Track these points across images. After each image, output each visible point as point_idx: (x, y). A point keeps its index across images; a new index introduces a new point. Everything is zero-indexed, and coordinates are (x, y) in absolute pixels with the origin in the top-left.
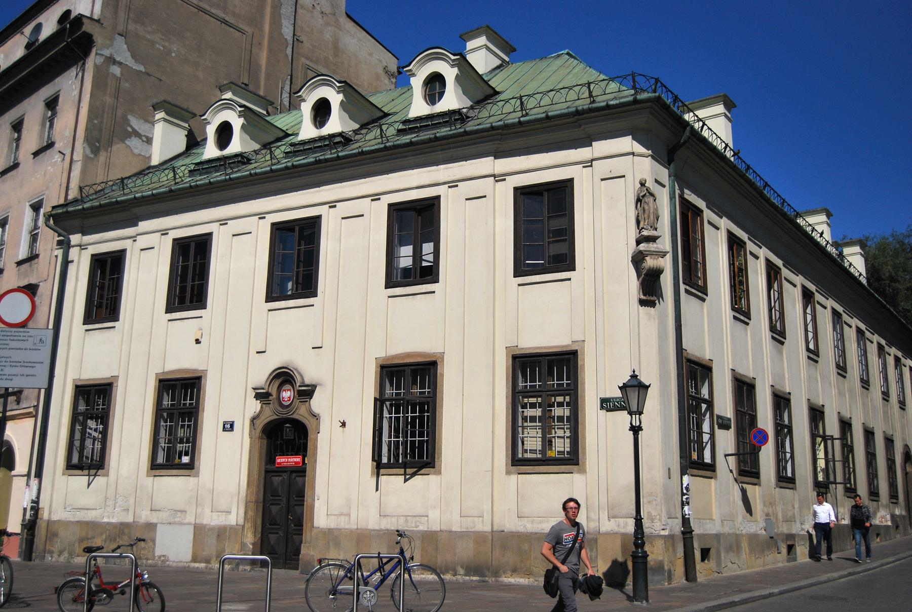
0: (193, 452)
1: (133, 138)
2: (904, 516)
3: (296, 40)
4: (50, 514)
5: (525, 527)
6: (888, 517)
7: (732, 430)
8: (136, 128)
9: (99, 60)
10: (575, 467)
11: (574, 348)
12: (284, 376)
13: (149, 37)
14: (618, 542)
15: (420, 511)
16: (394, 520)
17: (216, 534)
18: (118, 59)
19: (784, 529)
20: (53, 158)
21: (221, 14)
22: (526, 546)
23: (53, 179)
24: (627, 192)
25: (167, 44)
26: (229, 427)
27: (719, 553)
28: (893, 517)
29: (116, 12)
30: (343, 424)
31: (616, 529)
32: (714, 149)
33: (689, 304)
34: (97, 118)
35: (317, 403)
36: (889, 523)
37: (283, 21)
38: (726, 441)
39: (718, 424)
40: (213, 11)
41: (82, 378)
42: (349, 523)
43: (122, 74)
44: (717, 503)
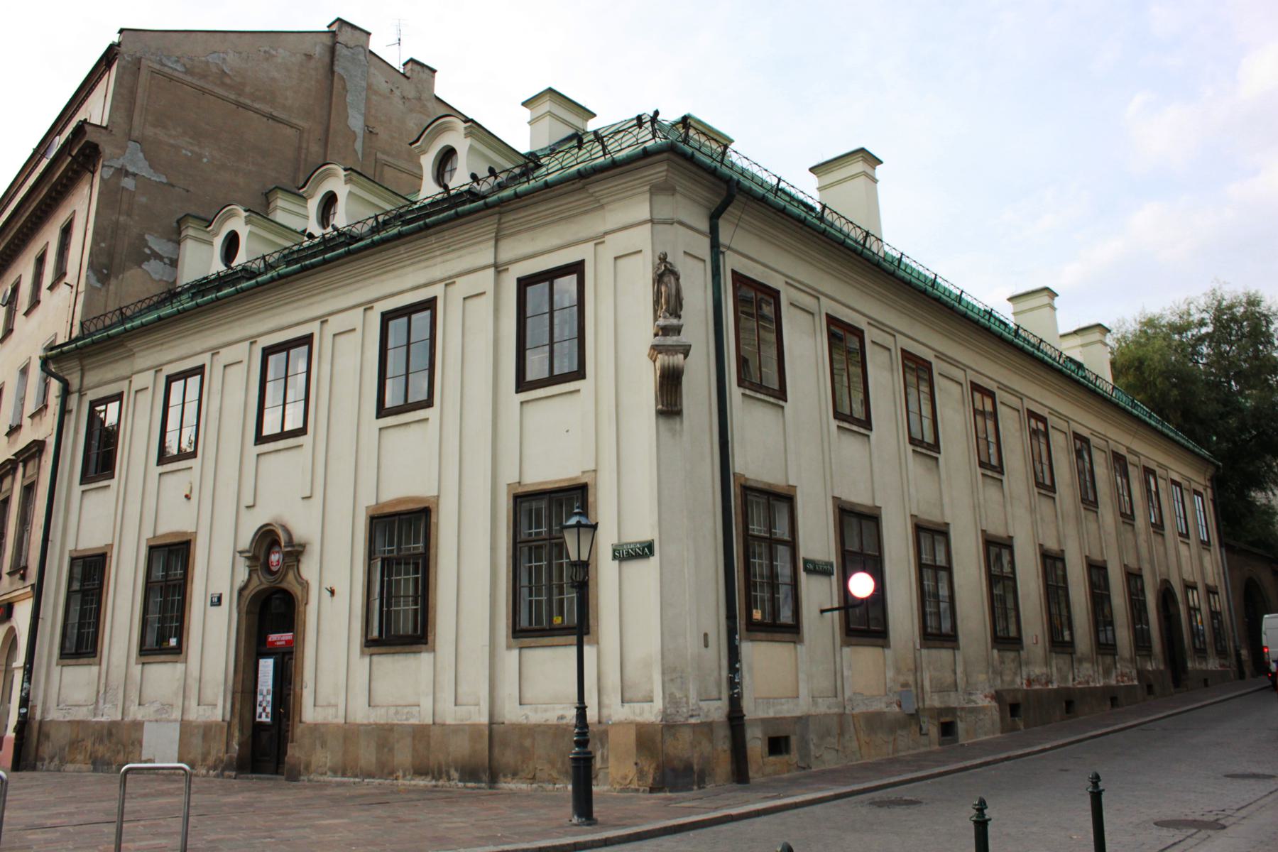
0: (180, 633)
1: (152, 261)
2: (1161, 672)
3: (370, 132)
4: (43, 712)
5: (527, 717)
6: (1134, 673)
7: (834, 578)
8: (156, 248)
9: (108, 173)
11: (583, 480)
12: (268, 538)
13: (172, 141)
14: (633, 737)
16: (383, 711)
17: (201, 731)
18: (131, 169)
19: (934, 701)
20: (63, 290)
21: (266, 108)
22: (528, 743)
23: (56, 316)
24: (641, 274)
25: (196, 149)
26: (217, 601)
27: (804, 743)
28: (1141, 674)
29: (130, 117)
30: (332, 592)
31: (632, 717)
33: (749, 417)
34: (104, 241)
35: (309, 569)
36: (1136, 683)
39: (806, 570)
40: (256, 105)
41: (81, 547)
42: (336, 717)
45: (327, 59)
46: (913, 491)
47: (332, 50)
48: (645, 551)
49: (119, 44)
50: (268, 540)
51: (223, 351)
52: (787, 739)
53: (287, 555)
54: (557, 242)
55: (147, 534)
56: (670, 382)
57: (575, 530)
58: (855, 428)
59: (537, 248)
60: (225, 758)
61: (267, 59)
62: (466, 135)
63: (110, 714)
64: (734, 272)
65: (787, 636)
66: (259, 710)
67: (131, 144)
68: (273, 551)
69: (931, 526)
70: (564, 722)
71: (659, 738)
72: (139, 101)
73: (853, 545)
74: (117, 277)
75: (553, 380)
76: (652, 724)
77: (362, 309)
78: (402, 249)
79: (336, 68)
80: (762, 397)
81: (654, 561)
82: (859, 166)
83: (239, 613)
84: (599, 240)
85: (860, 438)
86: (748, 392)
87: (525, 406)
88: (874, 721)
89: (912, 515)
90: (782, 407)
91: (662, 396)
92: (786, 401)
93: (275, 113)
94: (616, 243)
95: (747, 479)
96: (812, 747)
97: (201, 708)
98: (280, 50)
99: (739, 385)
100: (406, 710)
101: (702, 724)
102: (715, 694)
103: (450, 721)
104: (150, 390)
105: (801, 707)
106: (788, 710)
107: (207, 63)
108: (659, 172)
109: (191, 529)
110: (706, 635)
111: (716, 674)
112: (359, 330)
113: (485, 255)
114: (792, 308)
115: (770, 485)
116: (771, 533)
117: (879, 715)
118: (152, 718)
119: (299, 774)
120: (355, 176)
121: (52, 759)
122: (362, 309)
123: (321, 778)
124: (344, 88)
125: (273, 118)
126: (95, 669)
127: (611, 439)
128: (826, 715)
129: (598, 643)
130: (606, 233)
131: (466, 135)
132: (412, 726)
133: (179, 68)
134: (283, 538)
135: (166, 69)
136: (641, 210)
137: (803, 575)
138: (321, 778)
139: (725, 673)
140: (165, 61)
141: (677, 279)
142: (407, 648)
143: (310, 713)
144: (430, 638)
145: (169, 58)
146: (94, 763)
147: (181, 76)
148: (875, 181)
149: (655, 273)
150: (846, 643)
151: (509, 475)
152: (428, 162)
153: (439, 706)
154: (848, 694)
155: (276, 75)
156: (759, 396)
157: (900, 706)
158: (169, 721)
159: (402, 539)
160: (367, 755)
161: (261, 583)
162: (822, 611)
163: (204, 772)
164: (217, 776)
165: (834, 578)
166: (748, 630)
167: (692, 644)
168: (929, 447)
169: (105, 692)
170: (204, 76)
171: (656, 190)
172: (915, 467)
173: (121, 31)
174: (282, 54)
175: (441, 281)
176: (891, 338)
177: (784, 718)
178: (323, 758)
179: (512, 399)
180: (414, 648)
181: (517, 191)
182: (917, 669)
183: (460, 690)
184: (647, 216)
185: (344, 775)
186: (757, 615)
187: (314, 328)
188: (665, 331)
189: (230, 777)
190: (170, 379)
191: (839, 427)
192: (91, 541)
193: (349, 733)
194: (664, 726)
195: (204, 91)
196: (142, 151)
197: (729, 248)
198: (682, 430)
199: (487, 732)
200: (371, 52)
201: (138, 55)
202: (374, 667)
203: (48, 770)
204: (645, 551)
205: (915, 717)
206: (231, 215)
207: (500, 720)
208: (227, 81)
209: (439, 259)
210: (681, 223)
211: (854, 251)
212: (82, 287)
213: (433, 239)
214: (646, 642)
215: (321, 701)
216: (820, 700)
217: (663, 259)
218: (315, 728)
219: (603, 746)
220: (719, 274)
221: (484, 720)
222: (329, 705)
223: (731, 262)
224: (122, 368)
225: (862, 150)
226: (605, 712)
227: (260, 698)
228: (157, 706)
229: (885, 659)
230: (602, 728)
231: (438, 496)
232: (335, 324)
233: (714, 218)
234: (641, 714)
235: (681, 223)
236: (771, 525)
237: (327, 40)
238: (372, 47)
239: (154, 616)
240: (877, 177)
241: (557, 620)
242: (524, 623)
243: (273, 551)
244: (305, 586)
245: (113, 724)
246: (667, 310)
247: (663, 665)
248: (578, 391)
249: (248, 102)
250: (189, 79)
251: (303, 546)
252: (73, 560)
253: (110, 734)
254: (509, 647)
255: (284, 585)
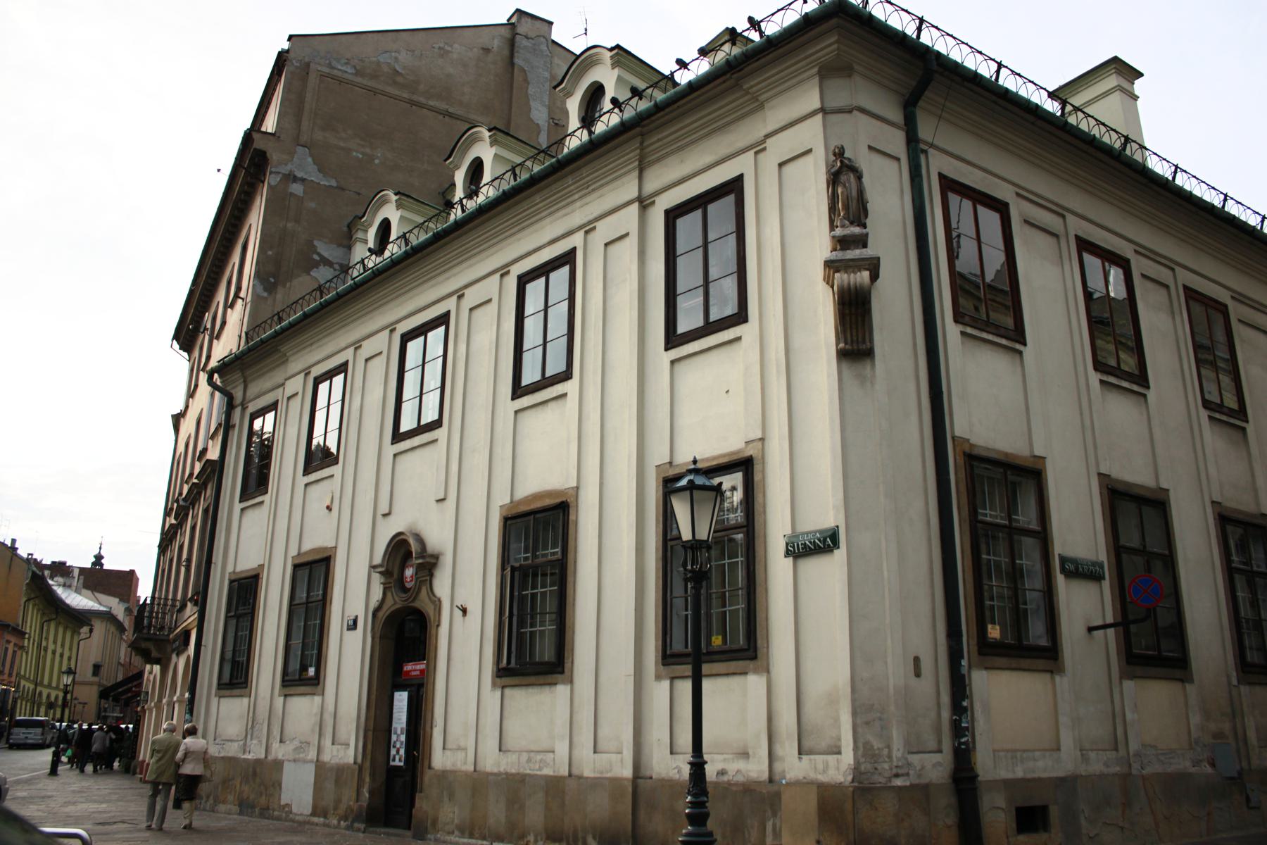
7: (1106, 584)
8: (326, 254)
10: (751, 664)
13: (342, 144)
15: (545, 745)
18: (299, 174)
21: (443, 106)
24: (811, 182)
25: (368, 150)
26: (353, 626)
29: (299, 122)
30: (464, 611)
31: (812, 775)
32: (975, 77)
33: (977, 373)
35: (442, 585)
37: (532, 103)
38: (1082, 607)
39: (1063, 570)
40: (431, 103)
41: (238, 569)
42: (465, 763)
43: (304, 192)
44: (1028, 723)
45: (506, 52)
46: (1212, 471)
47: (512, 43)
48: (826, 543)
49: (287, 51)
50: (402, 552)
51: (364, 344)
52: (1044, 809)
53: (420, 567)
54: (709, 159)
55: (293, 552)
56: (854, 312)
57: (688, 493)
58: (1125, 384)
59: (686, 172)
60: (355, 808)
61: (442, 56)
62: (614, 66)
63: (256, 752)
64: (940, 175)
65: (1041, 663)
66: (393, 752)
67: (300, 149)
68: (407, 562)
69: (1241, 517)
70: (725, 778)
71: (848, 806)
72: (307, 106)
73: (1131, 538)
74: (284, 286)
75: (710, 328)
76: (839, 786)
77: (497, 276)
78: (537, 198)
79: (516, 61)
80: (990, 337)
81: (840, 555)
82: (1112, 81)
83: (373, 638)
84: (758, 147)
85: (1134, 397)
86: (969, 330)
87: (677, 366)
88: (1174, 785)
89: (1213, 502)
90: (1020, 353)
91: (844, 332)
92: (1025, 344)
93: (451, 110)
94: (780, 147)
95: (972, 446)
96: (1083, 822)
97: (335, 747)
98: (456, 46)
99: (956, 321)
100: (539, 757)
101: (912, 786)
102: (932, 745)
103: (588, 773)
104: (300, 395)
105: (1065, 763)
106: (1044, 768)
107: (378, 63)
108: (827, 46)
109: (331, 544)
110: (917, 660)
111: (933, 714)
112: (495, 300)
113: (628, 189)
114: (1027, 228)
115: (1006, 454)
116: (1010, 520)
117: (1183, 777)
118: (291, 758)
119: (426, 831)
120: (500, 136)
121: (208, 797)
122: (497, 276)
123: (448, 838)
124: (526, 81)
125: (450, 115)
126: (245, 700)
127: (780, 400)
128: (1102, 776)
129: (768, 672)
130: (768, 136)
131: (614, 66)
132: (546, 777)
133: (350, 70)
134: (414, 546)
135: (335, 72)
136: (810, 98)
137: (1060, 579)
138: (448, 838)
139: (946, 714)
140: (334, 63)
141: (859, 177)
142: (541, 679)
143: (440, 759)
144: (567, 666)
145: (338, 60)
146: (240, 805)
147: (350, 77)
148: (1135, 98)
149: (828, 172)
150: (1124, 675)
151: (659, 455)
152: (573, 106)
153: (576, 753)
154: (1134, 746)
155: (451, 70)
156: (985, 335)
157: (1213, 765)
158: (305, 761)
159: (539, 539)
160: (496, 813)
161: (395, 603)
162: (1091, 629)
163: (335, 822)
164: (347, 828)
165: (1106, 584)
166: (980, 653)
167: (895, 673)
168: (1231, 412)
169: (253, 727)
170: (374, 76)
171: (827, 73)
172: (1213, 439)
173: (290, 38)
174: (457, 50)
175: (580, 228)
176: (1169, 273)
177: (1039, 780)
178: (451, 813)
179: (661, 358)
180: (549, 678)
181: (666, 112)
182: (1235, 713)
183: (602, 733)
184: (816, 104)
185: (471, 836)
186: (994, 632)
187: (450, 304)
188: (842, 243)
189: (359, 830)
190: (318, 381)
191: (1101, 381)
192: (246, 562)
193: (479, 782)
194: (856, 789)
195: (375, 92)
196: (311, 155)
197: (932, 145)
198: (874, 376)
199: (630, 789)
200: (554, 42)
201: (307, 60)
202: (506, 702)
203: (204, 810)
204: (826, 543)
205: (1237, 781)
206: (384, 201)
207: (648, 774)
208: (400, 79)
209: (578, 204)
210: (863, 111)
211: (1107, 150)
212: (249, 299)
213: (570, 180)
214: (831, 669)
215: (449, 745)
216: (1092, 755)
217: (839, 153)
218: (444, 775)
219: (775, 814)
220: (920, 175)
221: (628, 772)
222: (459, 748)
223: (936, 164)
224: (277, 377)
225: (1115, 60)
226: (778, 767)
227: (394, 738)
228: (296, 743)
229: (1186, 696)
230: (773, 788)
231: (577, 488)
232: (472, 297)
233: (909, 106)
234: (825, 771)
235: (863, 111)
236: (1011, 509)
237: (506, 32)
238: (554, 37)
239: (297, 642)
240: (1137, 93)
241: (717, 641)
242: (678, 646)
243: (407, 562)
244: (438, 604)
245: (258, 761)
246: (847, 217)
247: (853, 701)
248: (739, 339)
249: (422, 100)
250: (359, 80)
251: (436, 557)
252: (231, 582)
253: (255, 774)
254: (658, 677)
255: (417, 604)
